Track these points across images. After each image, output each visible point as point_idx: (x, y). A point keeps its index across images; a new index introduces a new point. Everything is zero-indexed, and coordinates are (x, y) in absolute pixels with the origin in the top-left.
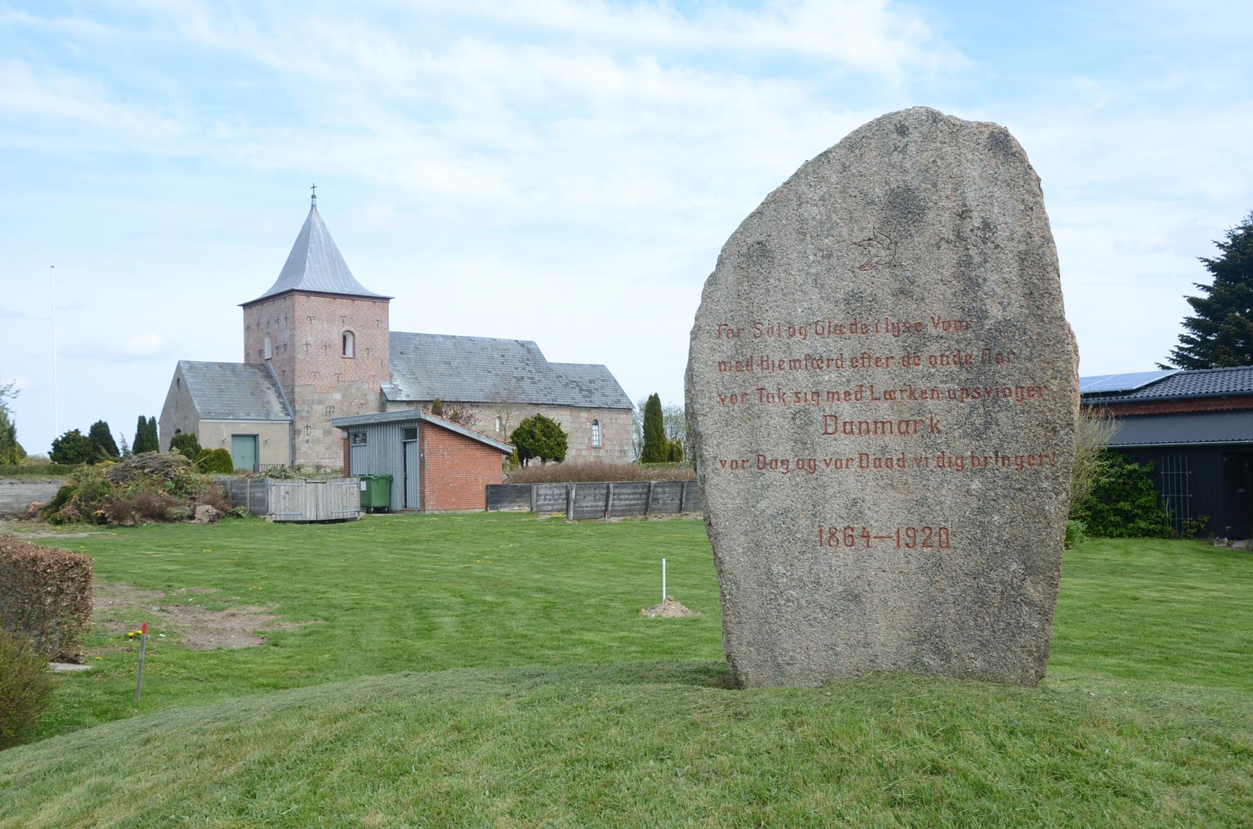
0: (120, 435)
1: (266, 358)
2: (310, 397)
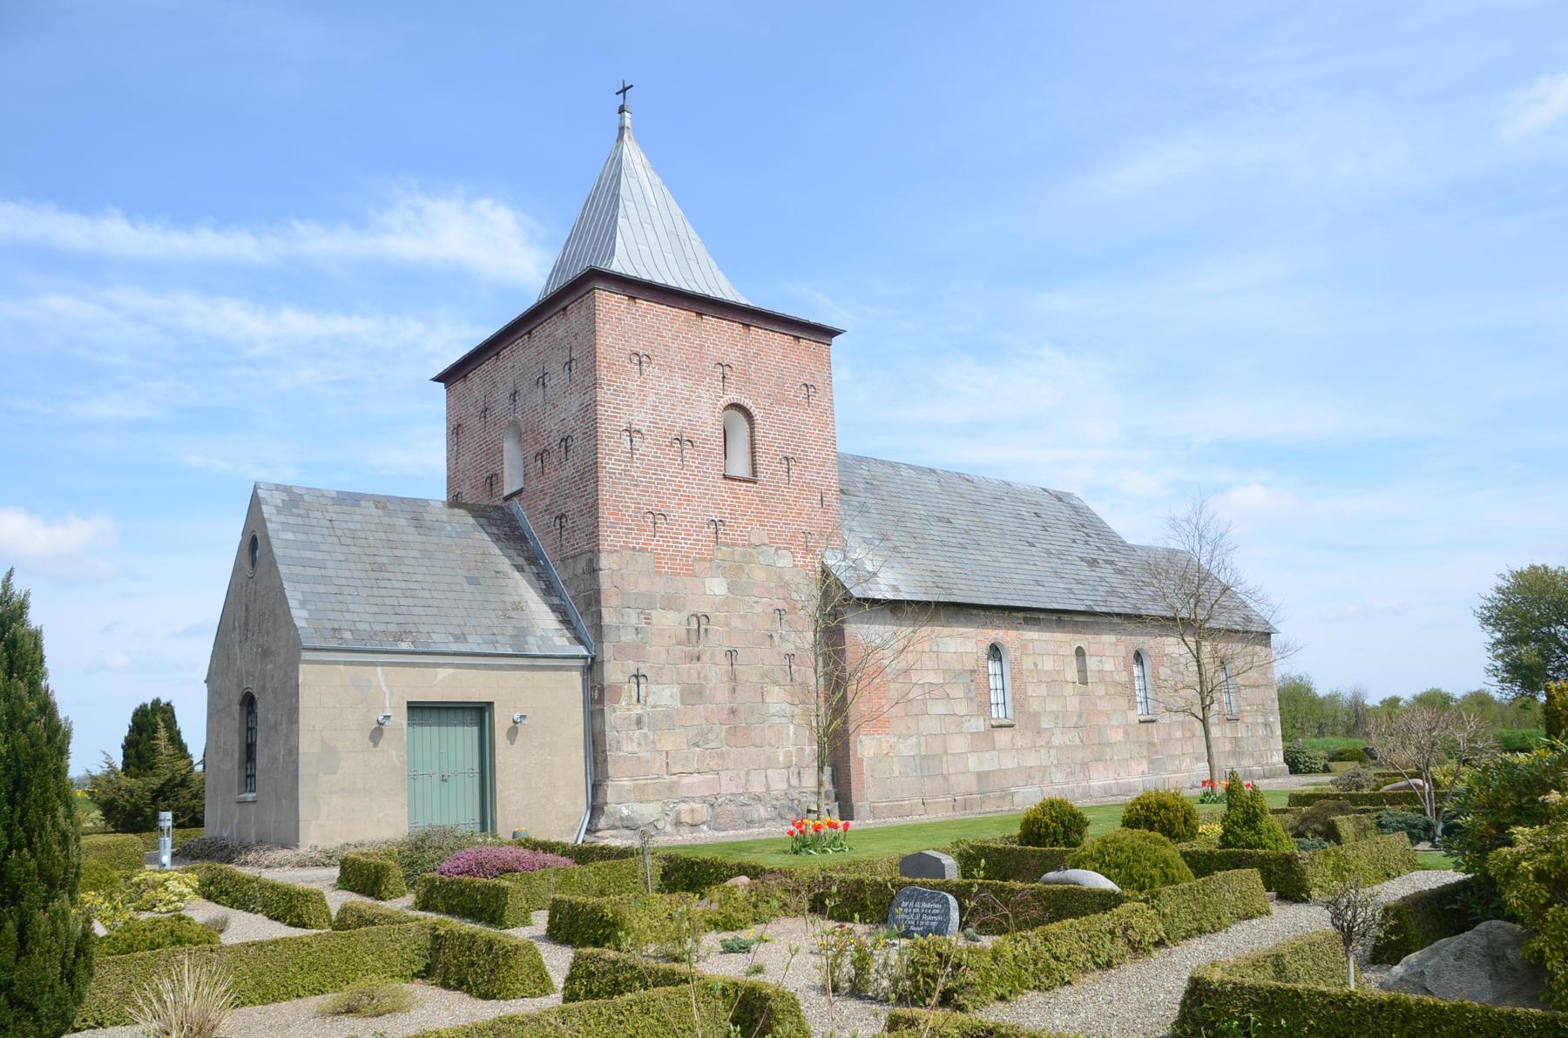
0: (102, 754)
1: (506, 493)
2: (643, 585)
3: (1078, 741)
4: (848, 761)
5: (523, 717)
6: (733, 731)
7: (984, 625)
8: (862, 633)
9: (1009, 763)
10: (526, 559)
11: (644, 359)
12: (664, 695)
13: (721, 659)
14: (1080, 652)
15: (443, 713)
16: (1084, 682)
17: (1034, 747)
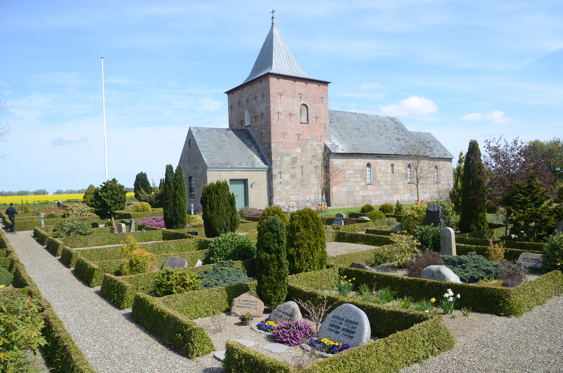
1: (246, 125)
2: (281, 151)
3: (390, 188)
4: (330, 192)
5: (255, 182)
6: (302, 185)
7: (366, 158)
8: (335, 162)
9: (371, 193)
10: (253, 143)
11: (281, 94)
12: (286, 177)
13: (300, 168)
14: (392, 165)
15: (238, 181)
16: (393, 173)
17: (378, 190)
